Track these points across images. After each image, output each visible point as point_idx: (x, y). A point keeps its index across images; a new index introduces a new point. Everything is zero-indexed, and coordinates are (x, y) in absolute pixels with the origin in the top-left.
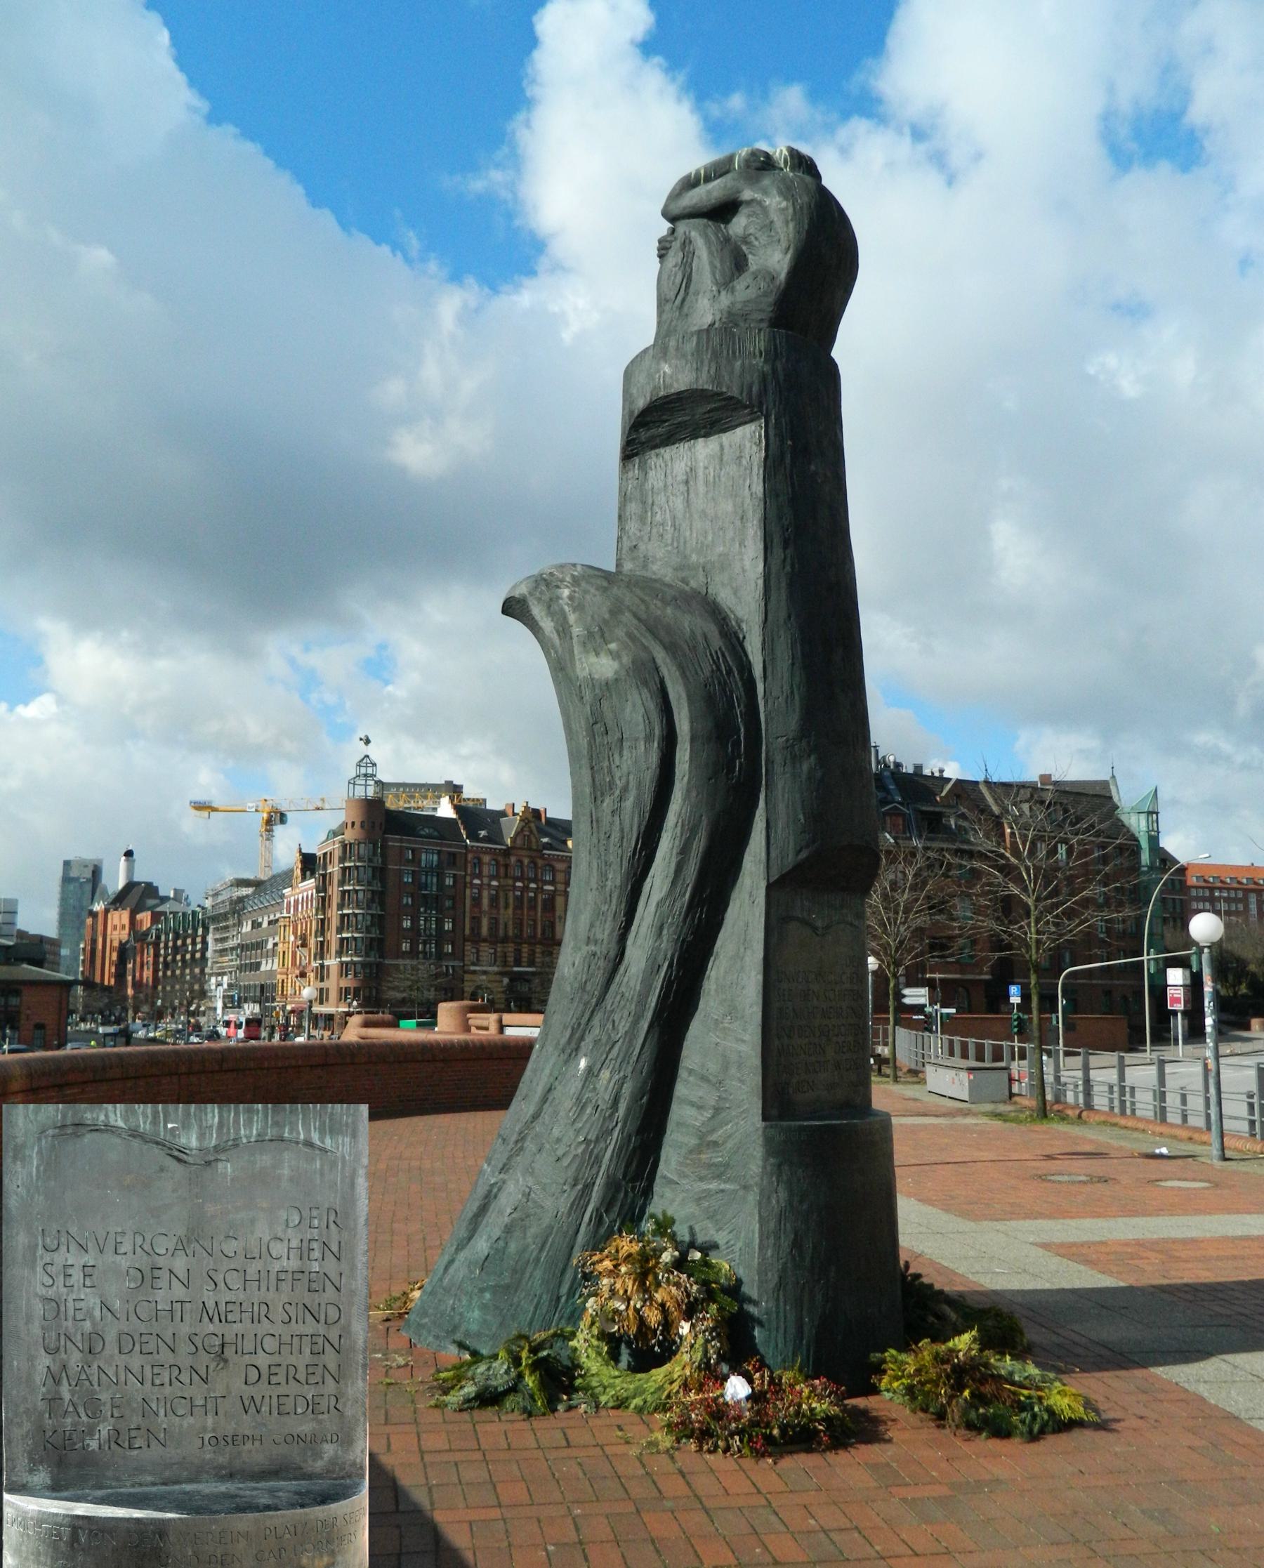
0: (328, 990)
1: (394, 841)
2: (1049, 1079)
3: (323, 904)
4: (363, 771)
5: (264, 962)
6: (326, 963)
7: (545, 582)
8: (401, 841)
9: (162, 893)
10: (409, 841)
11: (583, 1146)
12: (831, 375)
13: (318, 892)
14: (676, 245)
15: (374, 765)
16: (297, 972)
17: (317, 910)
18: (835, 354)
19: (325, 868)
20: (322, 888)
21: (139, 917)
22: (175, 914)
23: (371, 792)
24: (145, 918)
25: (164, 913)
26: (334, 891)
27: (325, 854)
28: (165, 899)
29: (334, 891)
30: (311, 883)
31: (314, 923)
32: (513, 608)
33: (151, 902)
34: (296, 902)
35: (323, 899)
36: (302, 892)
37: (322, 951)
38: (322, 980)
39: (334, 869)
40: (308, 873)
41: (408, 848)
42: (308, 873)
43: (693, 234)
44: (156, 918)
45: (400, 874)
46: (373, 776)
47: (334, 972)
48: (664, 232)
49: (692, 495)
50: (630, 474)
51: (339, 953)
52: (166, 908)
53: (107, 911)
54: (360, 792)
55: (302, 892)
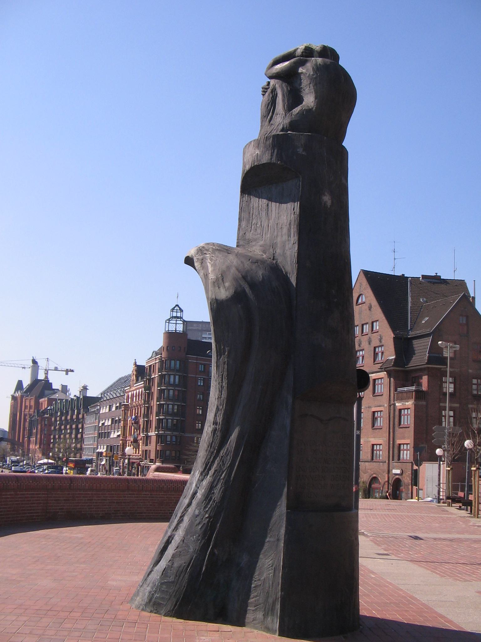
0: (150, 451)
1: (192, 359)
2: (212, 458)
3: (149, 395)
4: (175, 314)
5: (113, 432)
6: (150, 434)
7: (201, 251)
8: (197, 359)
9: (54, 387)
10: (200, 359)
11: (208, 519)
12: (340, 157)
13: (145, 390)
14: (269, 90)
15: (181, 311)
16: (132, 439)
17: (145, 401)
18: (346, 143)
19: (150, 375)
20: (148, 388)
21: (41, 400)
22: (61, 400)
23: (180, 328)
24: (44, 401)
25: (55, 400)
26: (155, 389)
27: (150, 366)
28: (55, 391)
29: (155, 389)
30: (141, 384)
31: (143, 409)
32: (189, 261)
33: (47, 392)
34: (133, 395)
35: (149, 394)
36: (136, 389)
37: (147, 429)
38: (147, 445)
39: (155, 375)
40: (140, 378)
41: (201, 364)
42: (140, 378)
43: (277, 86)
44: (50, 402)
45: (196, 380)
46: (181, 318)
47: (154, 439)
48: (265, 84)
49: (270, 211)
50: (244, 199)
51: (157, 428)
52: (56, 396)
53: (22, 397)
54: (172, 328)
55: (136, 389)
